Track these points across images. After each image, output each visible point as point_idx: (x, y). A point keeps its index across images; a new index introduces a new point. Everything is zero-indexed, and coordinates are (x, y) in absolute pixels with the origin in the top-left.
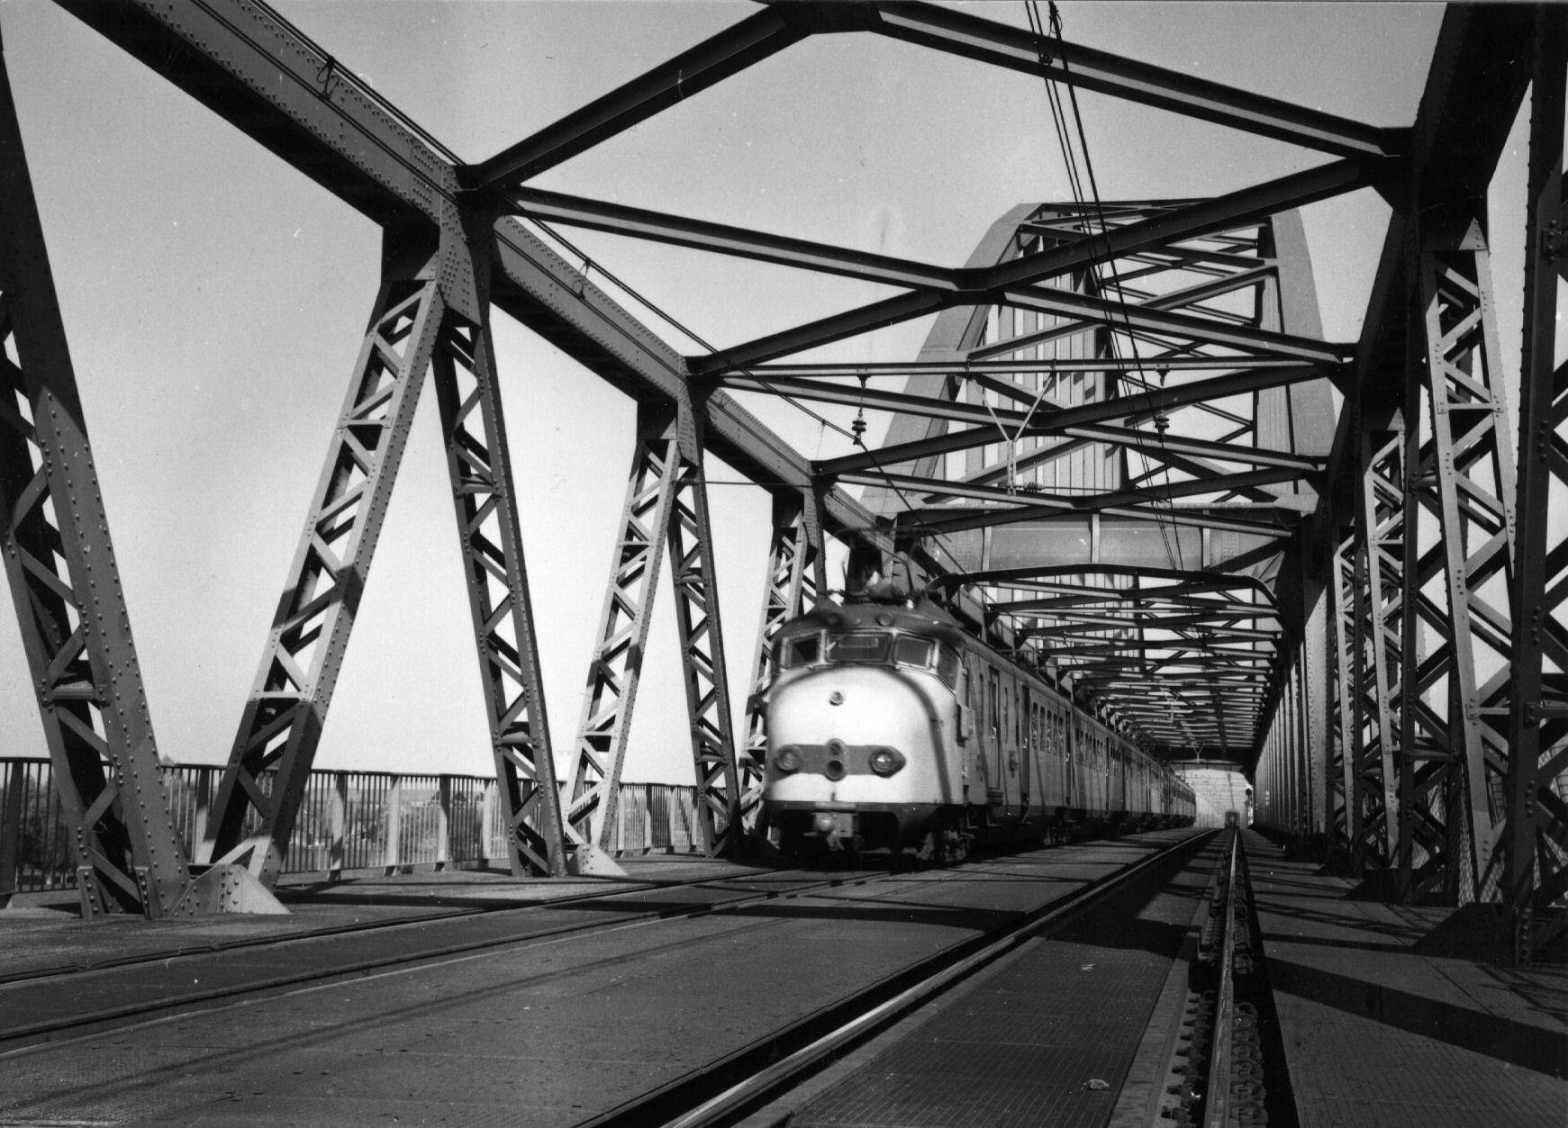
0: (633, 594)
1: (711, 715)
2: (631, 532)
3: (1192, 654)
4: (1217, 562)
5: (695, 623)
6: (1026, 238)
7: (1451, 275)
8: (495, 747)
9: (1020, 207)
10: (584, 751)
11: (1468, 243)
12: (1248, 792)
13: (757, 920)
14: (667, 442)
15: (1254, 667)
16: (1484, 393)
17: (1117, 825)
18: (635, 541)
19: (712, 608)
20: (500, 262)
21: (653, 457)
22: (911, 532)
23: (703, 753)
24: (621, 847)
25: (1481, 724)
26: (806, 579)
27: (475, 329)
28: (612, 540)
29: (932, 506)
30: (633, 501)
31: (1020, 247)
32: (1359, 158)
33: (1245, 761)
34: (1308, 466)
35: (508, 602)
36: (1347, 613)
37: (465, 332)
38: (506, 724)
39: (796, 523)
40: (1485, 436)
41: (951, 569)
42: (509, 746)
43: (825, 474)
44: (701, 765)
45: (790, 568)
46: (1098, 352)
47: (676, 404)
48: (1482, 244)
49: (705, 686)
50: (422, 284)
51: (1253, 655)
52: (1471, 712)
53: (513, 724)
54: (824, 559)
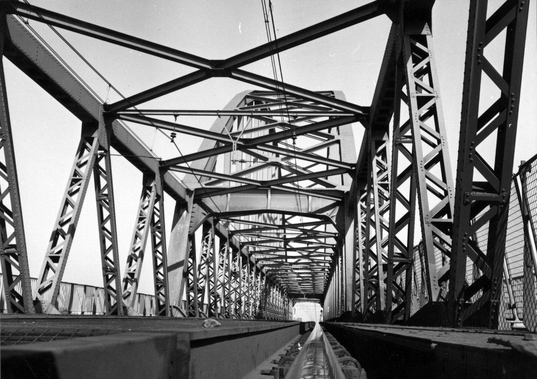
0: (75, 199)
1: (110, 255)
2: (76, 174)
3: (303, 261)
4: (314, 210)
5: (105, 217)
6: (249, 101)
7: (418, 45)
10: (48, 263)
11: (424, 32)
12: (321, 311)
14: (93, 138)
15: (325, 266)
16: (430, 89)
18: (78, 177)
19: (112, 210)
20: (10, 37)
21: (88, 144)
22: (199, 196)
23: (106, 271)
25: (431, 225)
26: (155, 207)
28: (68, 176)
29: (208, 187)
31: (246, 104)
32: (362, 115)
33: (321, 298)
34: (349, 167)
36: (363, 223)
38: (5, 245)
39: (152, 185)
40: (430, 108)
41: (215, 210)
43: (165, 166)
44: (106, 277)
45: (149, 201)
48: (430, 33)
49: (108, 243)
51: (324, 262)
52: (427, 220)
53: (8, 245)
54: (163, 200)
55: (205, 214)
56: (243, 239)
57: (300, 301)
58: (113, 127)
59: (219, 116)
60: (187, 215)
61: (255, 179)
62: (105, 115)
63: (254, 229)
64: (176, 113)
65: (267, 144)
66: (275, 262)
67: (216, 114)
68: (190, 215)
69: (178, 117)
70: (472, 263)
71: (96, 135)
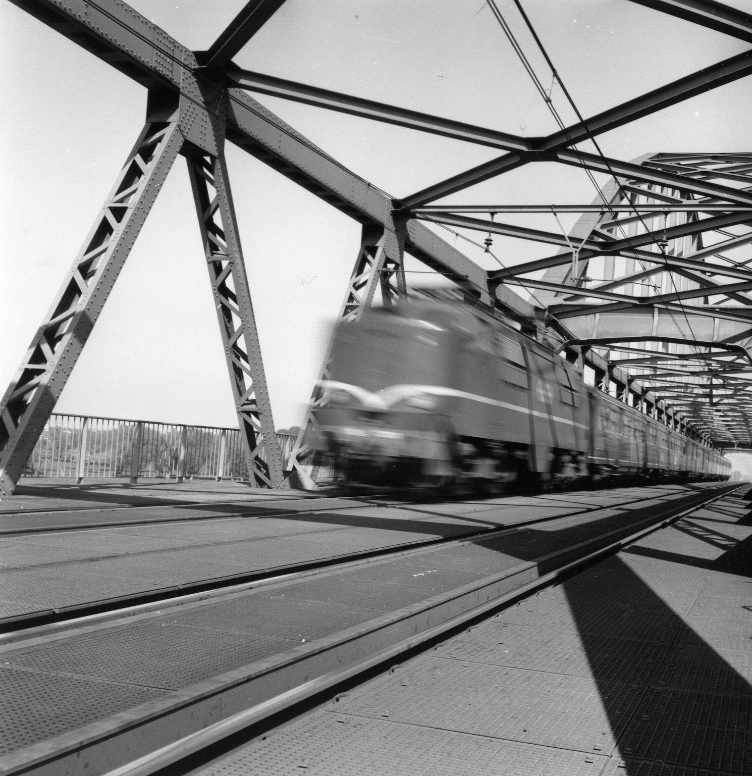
2: (351, 298)
4: (721, 339)
8: (238, 412)
9: (648, 154)
13: (433, 515)
14: (377, 247)
17: (683, 477)
18: (355, 303)
21: (370, 257)
22: (554, 316)
24: (81, 475)
27: (213, 158)
30: (354, 280)
35: (242, 329)
37: (208, 159)
38: (243, 400)
42: (248, 413)
47: (578, 354)
50: (168, 124)
55: (561, 342)
56: (633, 372)
57: (731, 451)
58: (409, 229)
59: (555, 213)
61: (630, 294)
64: (493, 210)
66: (738, 400)
69: (496, 216)
71: (381, 244)
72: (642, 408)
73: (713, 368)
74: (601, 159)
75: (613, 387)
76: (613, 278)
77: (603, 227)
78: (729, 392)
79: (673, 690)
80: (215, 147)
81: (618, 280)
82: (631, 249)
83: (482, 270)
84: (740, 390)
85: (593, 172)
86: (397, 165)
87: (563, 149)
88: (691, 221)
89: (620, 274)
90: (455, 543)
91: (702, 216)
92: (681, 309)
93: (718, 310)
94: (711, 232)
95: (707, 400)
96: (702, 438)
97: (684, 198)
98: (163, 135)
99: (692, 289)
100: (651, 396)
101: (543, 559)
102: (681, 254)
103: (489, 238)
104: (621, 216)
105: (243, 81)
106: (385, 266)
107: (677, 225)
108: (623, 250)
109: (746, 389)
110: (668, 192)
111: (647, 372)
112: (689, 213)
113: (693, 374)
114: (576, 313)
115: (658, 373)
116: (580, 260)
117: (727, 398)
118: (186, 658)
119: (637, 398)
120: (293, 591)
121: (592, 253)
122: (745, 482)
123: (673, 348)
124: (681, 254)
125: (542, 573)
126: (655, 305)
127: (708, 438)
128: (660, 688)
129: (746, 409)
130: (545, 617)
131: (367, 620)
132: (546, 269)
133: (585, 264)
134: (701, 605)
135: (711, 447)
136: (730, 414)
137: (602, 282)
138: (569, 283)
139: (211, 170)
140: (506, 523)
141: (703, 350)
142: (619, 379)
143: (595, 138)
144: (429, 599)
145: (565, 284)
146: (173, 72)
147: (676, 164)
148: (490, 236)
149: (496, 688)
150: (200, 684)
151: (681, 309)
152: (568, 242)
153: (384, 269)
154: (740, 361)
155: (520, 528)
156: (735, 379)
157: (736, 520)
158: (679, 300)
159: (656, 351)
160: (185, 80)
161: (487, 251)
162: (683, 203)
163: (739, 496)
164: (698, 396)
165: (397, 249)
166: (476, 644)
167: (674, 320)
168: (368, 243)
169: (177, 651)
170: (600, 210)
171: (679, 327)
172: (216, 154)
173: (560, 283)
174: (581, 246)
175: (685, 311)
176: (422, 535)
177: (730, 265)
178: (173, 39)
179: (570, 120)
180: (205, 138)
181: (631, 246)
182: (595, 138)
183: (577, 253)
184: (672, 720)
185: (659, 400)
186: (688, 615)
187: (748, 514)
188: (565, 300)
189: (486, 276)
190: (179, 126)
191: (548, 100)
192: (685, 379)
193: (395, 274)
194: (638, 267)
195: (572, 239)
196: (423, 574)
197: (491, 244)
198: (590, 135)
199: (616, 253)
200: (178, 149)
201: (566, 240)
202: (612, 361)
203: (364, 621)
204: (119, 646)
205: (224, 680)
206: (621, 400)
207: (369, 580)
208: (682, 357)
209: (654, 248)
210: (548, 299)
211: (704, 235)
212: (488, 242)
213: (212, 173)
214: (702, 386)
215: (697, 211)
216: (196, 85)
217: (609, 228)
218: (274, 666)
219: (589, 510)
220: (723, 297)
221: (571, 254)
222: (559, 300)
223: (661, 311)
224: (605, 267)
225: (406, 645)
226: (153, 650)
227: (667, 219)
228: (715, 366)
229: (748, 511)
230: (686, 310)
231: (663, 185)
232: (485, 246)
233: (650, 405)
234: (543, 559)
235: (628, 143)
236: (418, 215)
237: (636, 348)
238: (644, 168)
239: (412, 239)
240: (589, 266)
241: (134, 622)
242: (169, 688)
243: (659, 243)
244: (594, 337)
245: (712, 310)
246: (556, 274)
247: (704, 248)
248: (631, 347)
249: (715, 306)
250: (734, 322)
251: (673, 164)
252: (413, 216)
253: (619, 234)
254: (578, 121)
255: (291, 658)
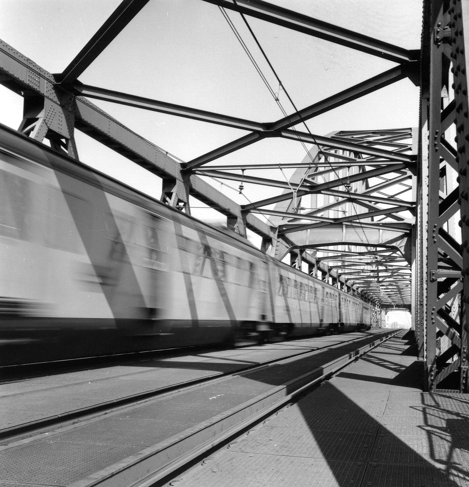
14: (172, 193)
17: (361, 327)
22: (282, 232)
27: (67, 140)
29: (290, 223)
34: (409, 205)
46: (325, 161)
48: (446, 95)
50: (37, 119)
56: (331, 264)
57: (392, 310)
59: (281, 169)
60: (272, 249)
62: (182, 172)
63: (343, 256)
64: (243, 168)
65: (332, 189)
66: (394, 278)
67: (278, 167)
68: (275, 248)
69: (245, 171)
70: (406, 342)
71: (174, 190)
72: (337, 286)
73: (378, 260)
74: (310, 135)
75: (319, 274)
76: (316, 207)
77: (309, 176)
78: (389, 274)
79: (383, 464)
80: (68, 132)
81: (320, 208)
82: (328, 189)
83: (237, 205)
84: (395, 272)
85: (305, 143)
86: (182, 142)
87: (285, 129)
88: (361, 172)
89: (320, 205)
90: (229, 377)
91: (368, 169)
92: (359, 225)
93: (381, 225)
94: (374, 178)
95: (376, 279)
96: (376, 304)
97: (357, 158)
98: (35, 126)
99: (364, 213)
100: (343, 278)
101: (288, 383)
102: (356, 190)
103: (242, 185)
104: (321, 169)
105: (84, 92)
106: (178, 204)
107: (353, 174)
108: (323, 190)
109: (398, 272)
110: (347, 154)
111: (340, 264)
112: (360, 166)
113: (367, 264)
114: (295, 230)
115: (346, 264)
116: (297, 196)
117: (389, 278)
118: (69, 464)
119: (334, 280)
120: (133, 413)
121: (304, 193)
122: (401, 328)
123: (354, 249)
124: (356, 190)
125: (288, 393)
126: (343, 223)
127: (378, 303)
128: (375, 464)
129: (399, 284)
130: (295, 421)
131: (184, 430)
132: (276, 203)
133: (300, 199)
134: (390, 407)
135: (379, 308)
136: (390, 287)
137: (310, 210)
138: (291, 211)
139: (66, 146)
140: (261, 362)
141: (372, 249)
142: (323, 269)
143: (305, 122)
144: (221, 413)
145: (288, 212)
146: (40, 87)
147: (351, 137)
148: (242, 184)
149: (273, 470)
150: (80, 481)
151: (359, 225)
152: (290, 186)
153: (177, 206)
154: (394, 255)
155: (270, 365)
156: (392, 266)
157: (401, 352)
158: (359, 219)
159: (337, 250)
160: (48, 91)
161: (240, 193)
162: (357, 161)
163: (400, 338)
164: (369, 277)
165: (185, 194)
166: (255, 441)
167: (356, 232)
168: (167, 191)
169: (62, 460)
170: (308, 166)
171: (359, 236)
172: (69, 137)
173: (285, 211)
174: (298, 188)
175: (362, 226)
176: (212, 372)
177: (386, 197)
178: (39, 67)
179: (291, 111)
180: (61, 127)
181: (328, 188)
182: (305, 122)
183: (296, 193)
184: (386, 484)
185: (348, 281)
186: (383, 414)
187: (407, 349)
188: (289, 221)
189: (240, 208)
190: (44, 120)
191: (277, 100)
192: (362, 267)
193: (184, 208)
194: (332, 200)
195: (292, 184)
196: (215, 397)
197: (243, 189)
198: (302, 120)
199: (319, 192)
200: (45, 135)
201: (289, 185)
202: (318, 258)
203: (182, 431)
204: (23, 458)
205: (96, 477)
206: (324, 282)
207: (181, 403)
208: (361, 254)
209: (342, 188)
210: (278, 222)
211: (369, 180)
212: (241, 188)
213: (67, 149)
214: (372, 271)
215: (365, 165)
216: (55, 95)
217: (313, 177)
218: (128, 465)
219: (313, 350)
220: (383, 216)
221: (292, 193)
222: (285, 222)
223: (347, 226)
224: (324, 200)
225: (211, 444)
226: (46, 460)
227: (350, 170)
228: (379, 258)
229: (407, 347)
230: (363, 225)
231: (344, 150)
232: (240, 190)
233: (342, 284)
234: (288, 383)
235: (324, 125)
236: (197, 172)
237: (332, 249)
238: (332, 140)
239: (193, 187)
240: (302, 200)
241: (31, 442)
242: (60, 485)
243: (345, 185)
244: (307, 244)
245: (377, 225)
246: (283, 206)
247: (370, 188)
248: (329, 249)
249: (379, 222)
250: (391, 231)
251: (349, 137)
252: (194, 173)
253: (320, 180)
254: (295, 112)
255: (139, 458)
